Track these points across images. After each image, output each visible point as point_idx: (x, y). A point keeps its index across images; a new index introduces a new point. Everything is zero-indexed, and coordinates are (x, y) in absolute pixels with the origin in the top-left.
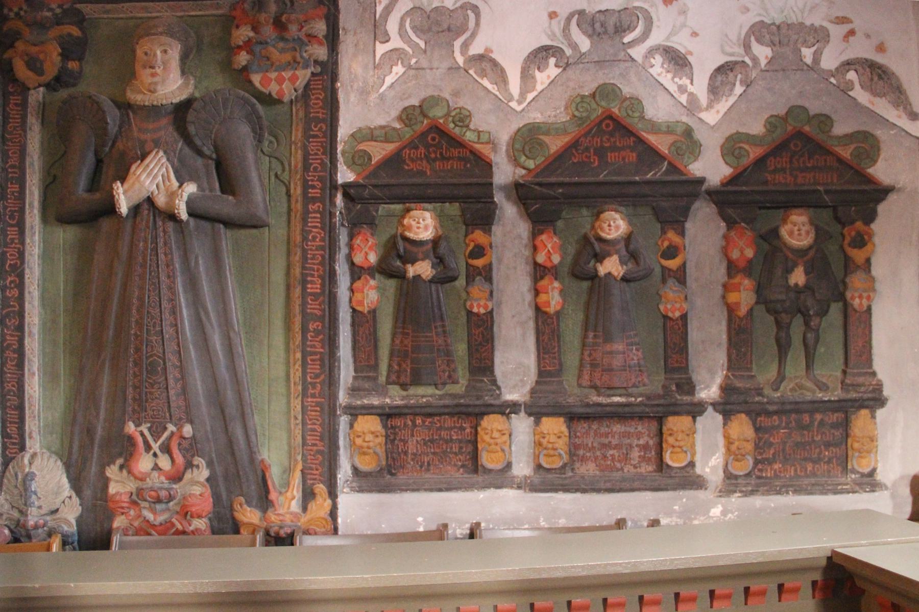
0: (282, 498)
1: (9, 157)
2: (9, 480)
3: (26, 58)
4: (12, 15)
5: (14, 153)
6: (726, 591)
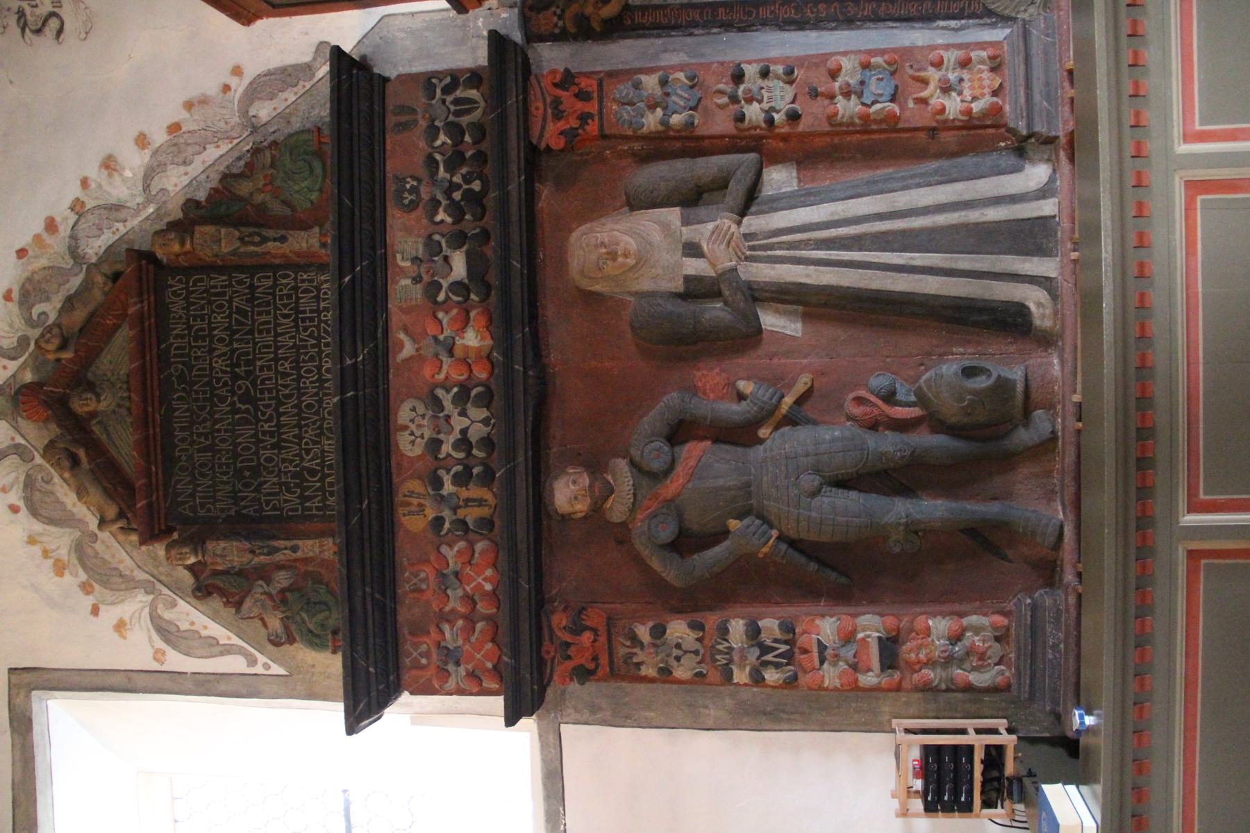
0: (570, 711)
1: (693, 20)
2: (1005, 9)
3: (600, 5)
4: (560, 23)
5: (688, 15)
6: (1131, 56)
